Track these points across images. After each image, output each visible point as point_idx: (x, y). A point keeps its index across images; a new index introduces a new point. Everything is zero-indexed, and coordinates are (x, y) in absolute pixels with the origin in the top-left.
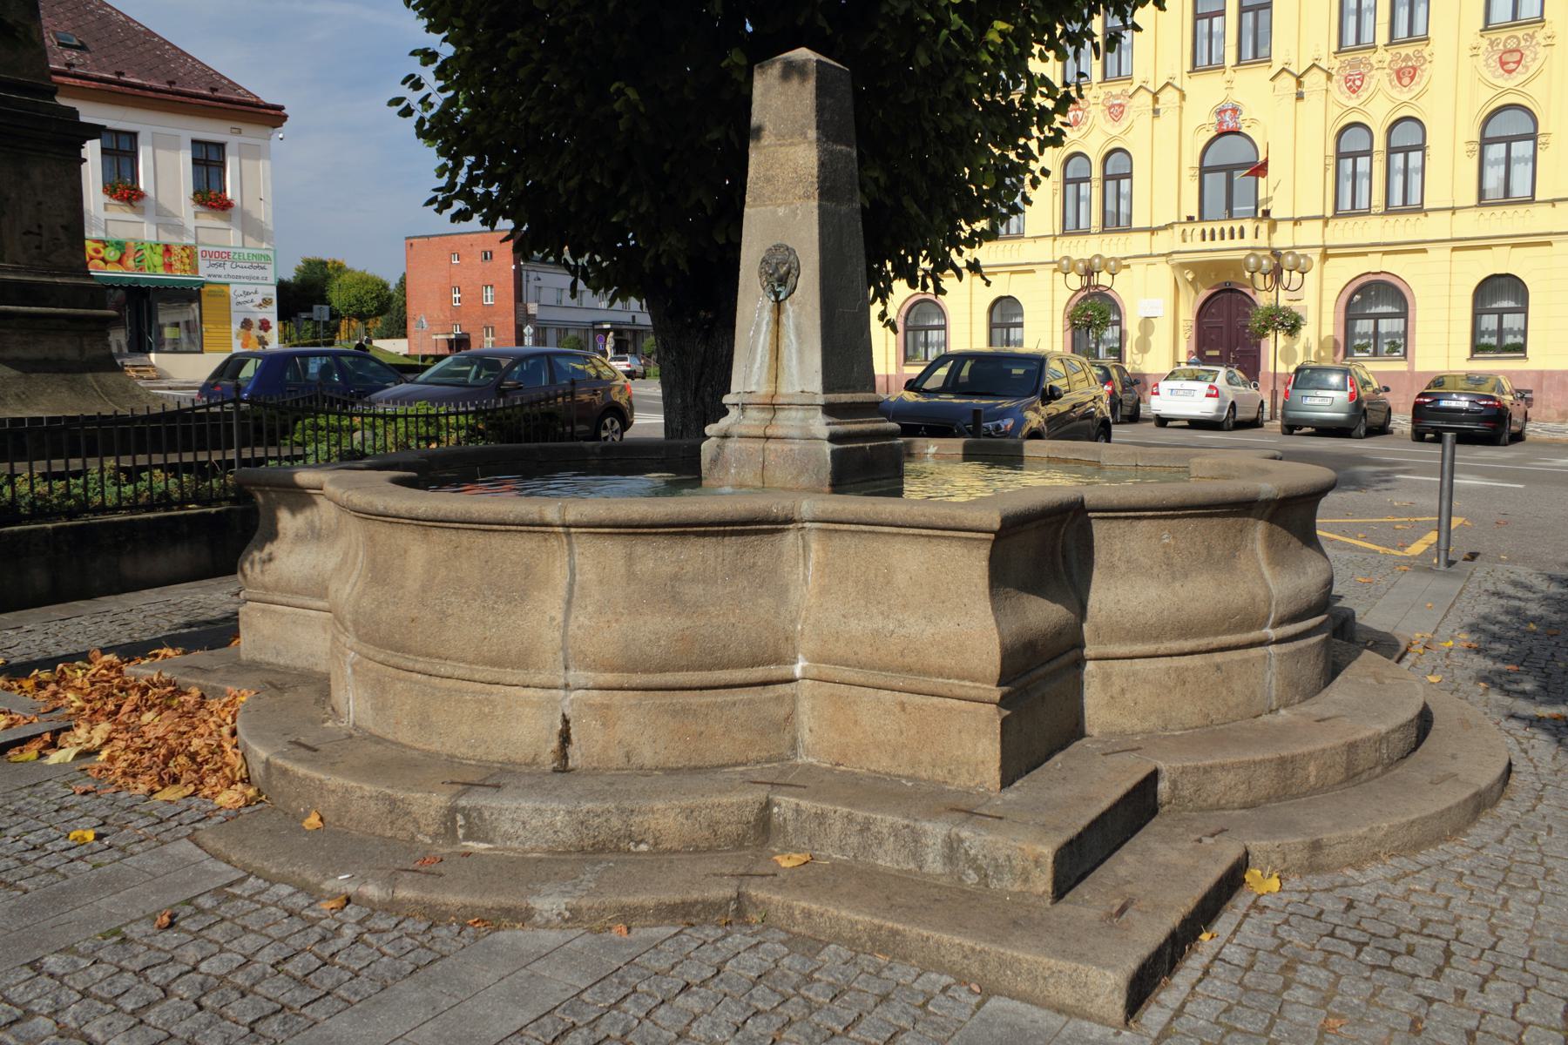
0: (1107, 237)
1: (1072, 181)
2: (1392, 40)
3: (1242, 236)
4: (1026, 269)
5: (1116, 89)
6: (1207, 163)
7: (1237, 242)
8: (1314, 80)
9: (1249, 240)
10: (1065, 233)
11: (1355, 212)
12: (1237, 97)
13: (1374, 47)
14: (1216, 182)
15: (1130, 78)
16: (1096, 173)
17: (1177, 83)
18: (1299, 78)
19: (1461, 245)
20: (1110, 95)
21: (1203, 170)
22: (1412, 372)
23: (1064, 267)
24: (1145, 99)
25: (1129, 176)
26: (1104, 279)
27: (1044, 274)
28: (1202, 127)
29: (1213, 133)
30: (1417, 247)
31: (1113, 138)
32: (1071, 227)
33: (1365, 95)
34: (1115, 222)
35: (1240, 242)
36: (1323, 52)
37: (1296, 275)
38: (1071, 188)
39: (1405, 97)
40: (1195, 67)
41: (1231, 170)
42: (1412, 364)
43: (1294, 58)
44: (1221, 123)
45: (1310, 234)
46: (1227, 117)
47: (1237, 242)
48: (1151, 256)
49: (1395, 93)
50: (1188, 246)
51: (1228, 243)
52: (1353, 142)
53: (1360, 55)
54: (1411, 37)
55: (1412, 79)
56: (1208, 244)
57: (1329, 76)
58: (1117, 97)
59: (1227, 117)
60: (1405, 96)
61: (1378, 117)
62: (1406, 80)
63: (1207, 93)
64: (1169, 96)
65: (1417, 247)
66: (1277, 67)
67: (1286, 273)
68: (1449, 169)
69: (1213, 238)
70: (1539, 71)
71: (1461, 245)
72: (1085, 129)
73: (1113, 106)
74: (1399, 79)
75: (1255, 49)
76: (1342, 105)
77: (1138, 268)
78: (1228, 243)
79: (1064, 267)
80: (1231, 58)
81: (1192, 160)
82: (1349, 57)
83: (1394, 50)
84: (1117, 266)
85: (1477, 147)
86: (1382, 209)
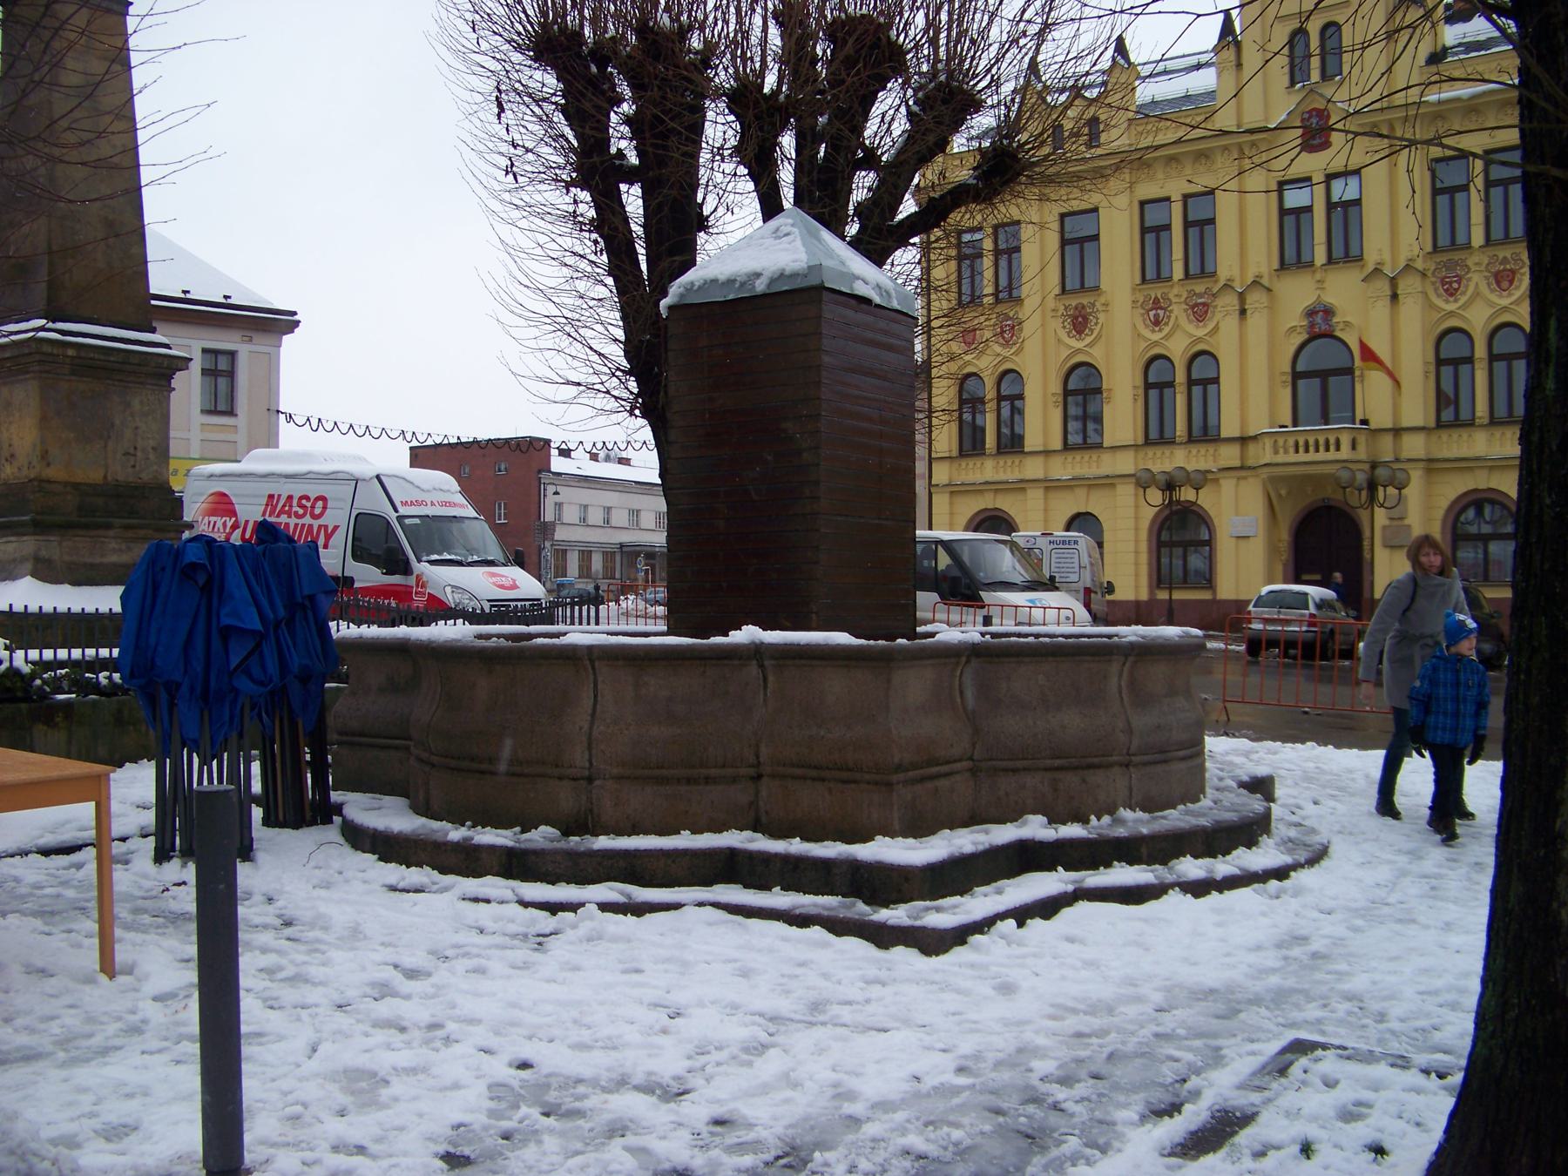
0: (1194, 449)
1: (1447, 362)
2: (1488, 240)
3: (1338, 448)
4: (1107, 482)
5: (1199, 287)
6: (1300, 368)
7: (1332, 455)
8: (1409, 285)
9: (1345, 453)
10: (1148, 442)
11: (1458, 423)
12: (1330, 299)
13: (1468, 246)
14: (1309, 388)
15: (1214, 274)
16: (1180, 377)
17: (1265, 281)
18: (1393, 281)
19: (1051, 486)
20: (1192, 293)
21: (1296, 376)
22: (1214, 601)
23: (1143, 482)
24: (1229, 302)
25: (1216, 381)
26: (1187, 494)
27: (1126, 492)
28: (1293, 329)
29: (1305, 336)
30: (1021, 486)
31: (1199, 340)
32: (1156, 436)
33: (1463, 300)
34: (1205, 433)
35: (1340, 452)
36: (1264, 270)
37: (1391, 490)
38: (1153, 393)
39: (1505, 302)
40: (1283, 266)
41: (1324, 373)
42: (1215, 593)
43: (1387, 257)
44: (1312, 325)
45: (1414, 446)
46: (1319, 318)
47: (1332, 455)
48: (1242, 468)
49: (1493, 298)
50: (1280, 458)
51: (1322, 455)
52: (1451, 349)
53: (1456, 256)
54: (1158, 277)
55: (1511, 282)
56: (1302, 457)
57: (1424, 275)
58: (1200, 295)
59: (1319, 318)
60: (1156, 337)
61: (1178, 349)
62: (1505, 284)
63: (1298, 294)
64: (1255, 299)
65: (1021, 486)
66: (1370, 267)
67: (1381, 489)
68: (1042, 421)
69: (1307, 451)
70: (1099, 337)
71: (1051, 486)
72: (1167, 330)
73: (1197, 305)
74: (1498, 283)
75: (1345, 253)
76: (1191, 335)
77: (1228, 485)
78: (1322, 455)
79: (1143, 482)
80: (1320, 256)
81: (1056, 387)
82: (1444, 257)
83: (1491, 251)
84: (1200, 480)
85: (1060, 399)
86: (1486, 421)
